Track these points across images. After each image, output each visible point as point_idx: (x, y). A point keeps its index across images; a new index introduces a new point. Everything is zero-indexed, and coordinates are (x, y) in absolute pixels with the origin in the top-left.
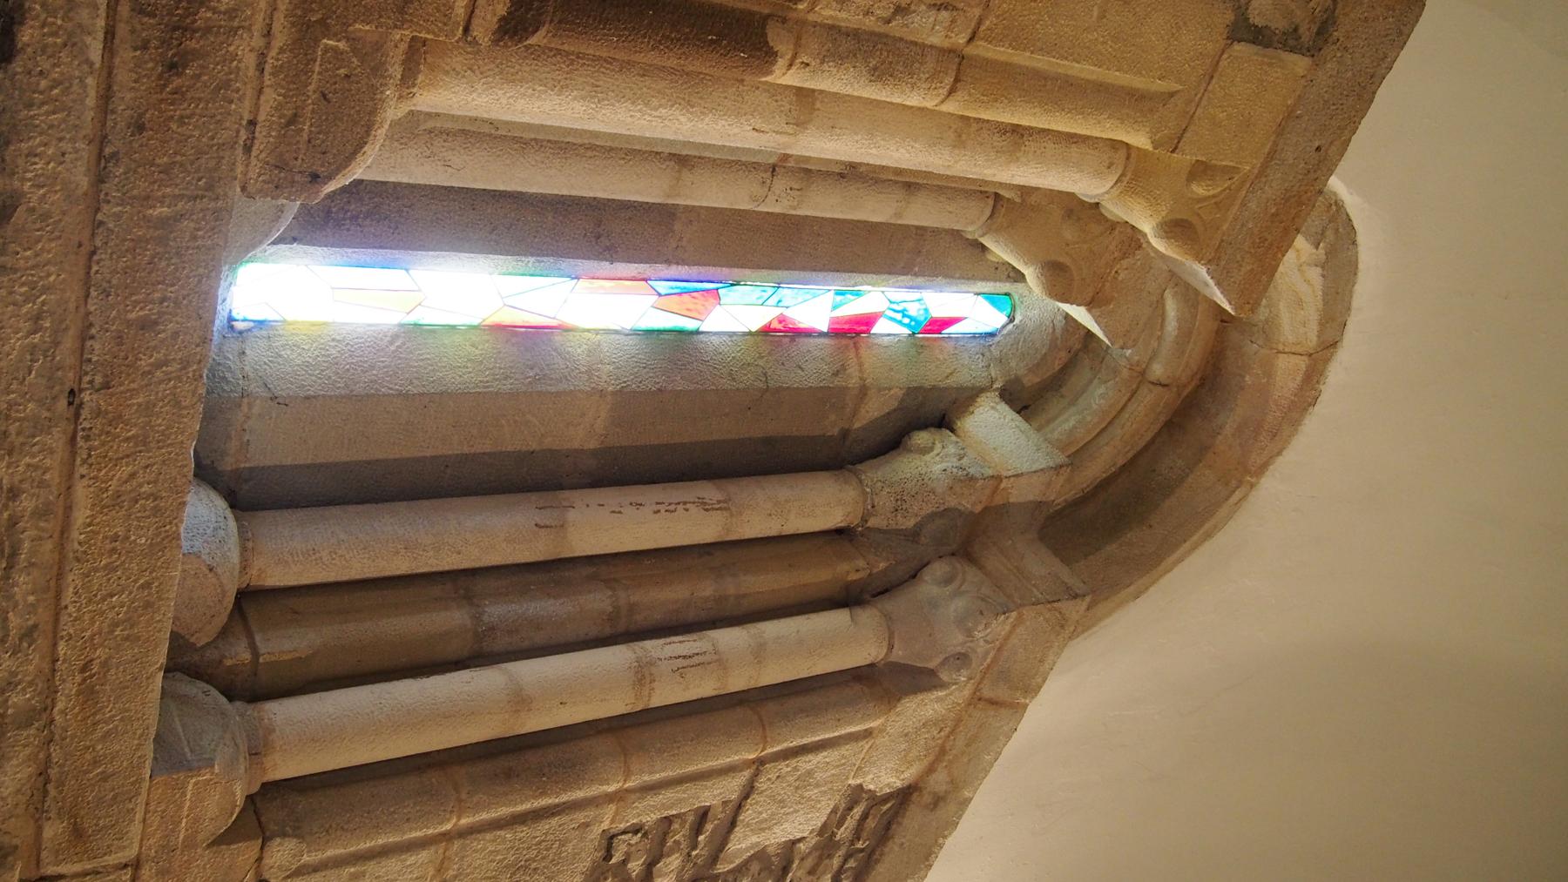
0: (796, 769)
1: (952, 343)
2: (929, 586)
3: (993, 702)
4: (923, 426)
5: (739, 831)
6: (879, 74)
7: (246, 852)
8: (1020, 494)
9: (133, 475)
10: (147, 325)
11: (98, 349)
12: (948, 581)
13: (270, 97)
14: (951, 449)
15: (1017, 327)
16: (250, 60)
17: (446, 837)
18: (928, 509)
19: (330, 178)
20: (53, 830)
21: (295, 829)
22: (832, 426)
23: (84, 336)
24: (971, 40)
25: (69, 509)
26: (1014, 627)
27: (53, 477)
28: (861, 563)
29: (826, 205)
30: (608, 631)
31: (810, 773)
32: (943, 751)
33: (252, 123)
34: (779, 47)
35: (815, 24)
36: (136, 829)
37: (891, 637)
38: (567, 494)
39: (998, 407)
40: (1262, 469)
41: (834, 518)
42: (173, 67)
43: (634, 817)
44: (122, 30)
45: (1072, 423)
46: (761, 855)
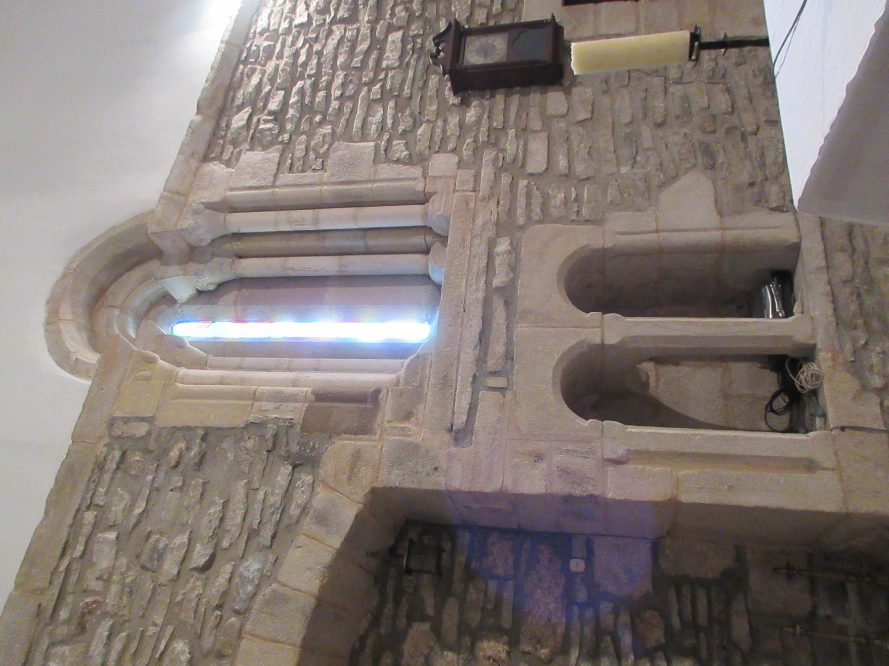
0: (258, 181)
1: (198, 319)
2: (208, 238)
3: (178, 193)
4: (209, 291)
5: (277, 160)
6: (281, 392)
7: (429, 189)
8: (174, 269)
9: (453, 293)
10: (451, 326)
11: (460, 321)
12: (202, 240)
13: (427, 373)
14: (200, 284)
15: (170, 326)
16: (431, 379)
17: (376, 181)
18: (210, 264)
19: (415, 358)
20: (472, 205)
21: (416, 193)
22: (246, 292)
23: (462, 323)
24: (253, 404)
25: (466, 285)
26: (177, 223)
27: (469, 293)
28: (235, 247)
29: (236, 360)
30: (325, 233)
31: (252, 178)
32: (195, 175)
33: (431, 367)
34: (311, 395)
35: (301, 402)
36: (454, 202)
37: (224, 223)
38: (338, 274)
39: (179, 298)
40: (64, 276)
41: (245, 262)
42: (445, 376)
43: (315, 176)
44: (455, 382)
45: (147, 293)
46: (265, 148)
